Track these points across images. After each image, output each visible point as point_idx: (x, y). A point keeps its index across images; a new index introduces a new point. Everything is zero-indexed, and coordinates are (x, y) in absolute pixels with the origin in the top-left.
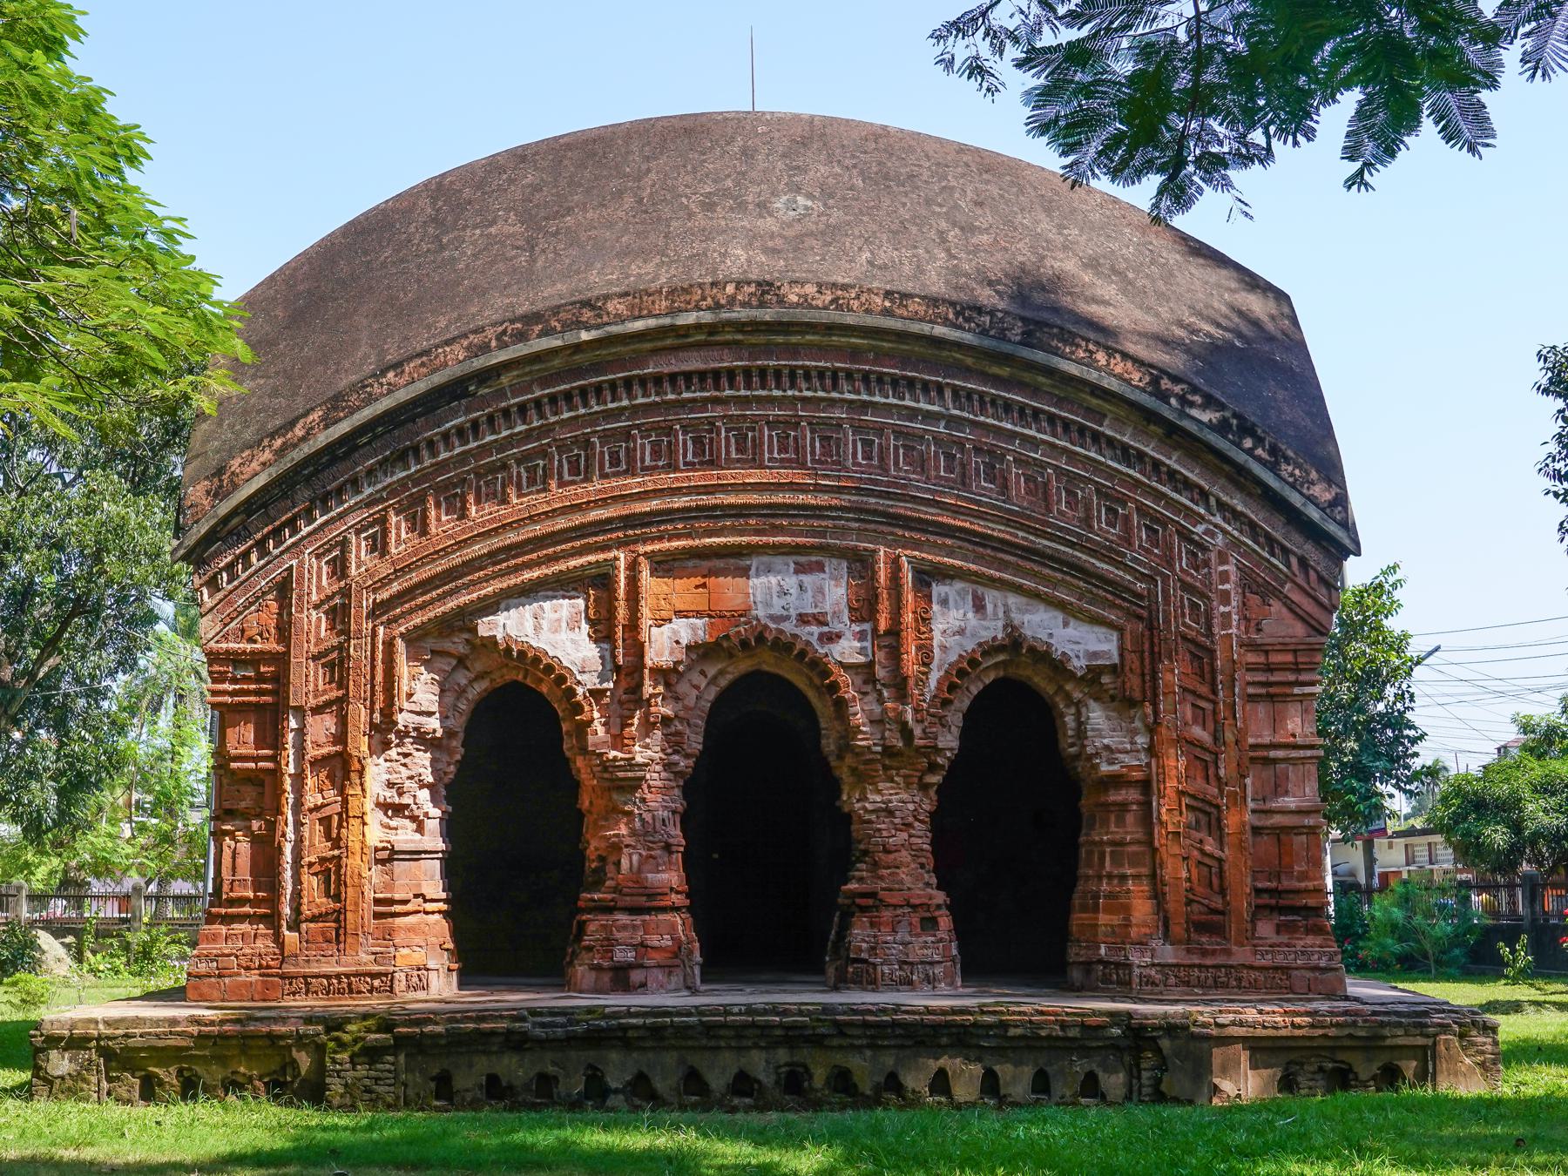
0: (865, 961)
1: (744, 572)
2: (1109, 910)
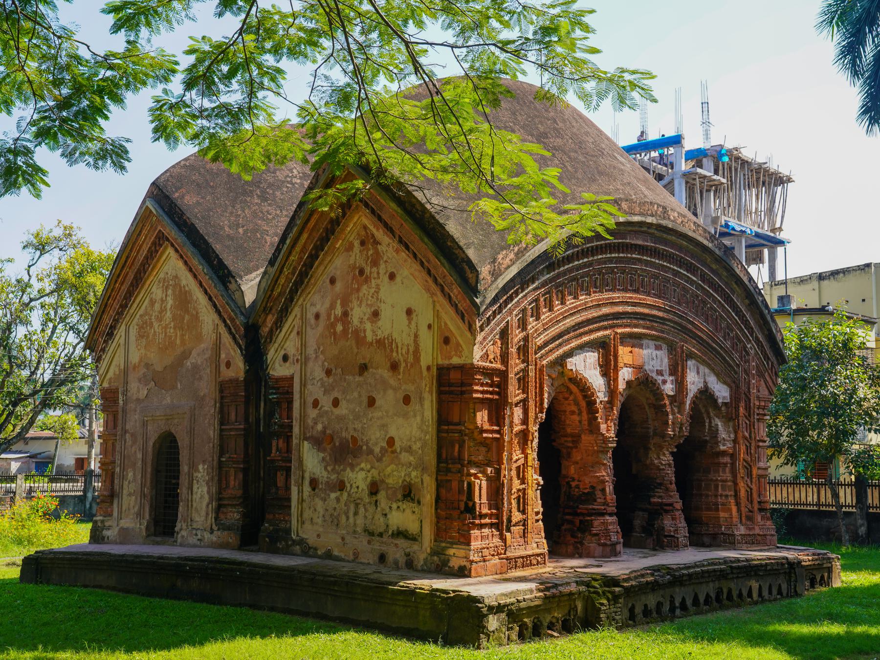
0: (673, 536)
1: (641, 346)
2: (724, 511)
